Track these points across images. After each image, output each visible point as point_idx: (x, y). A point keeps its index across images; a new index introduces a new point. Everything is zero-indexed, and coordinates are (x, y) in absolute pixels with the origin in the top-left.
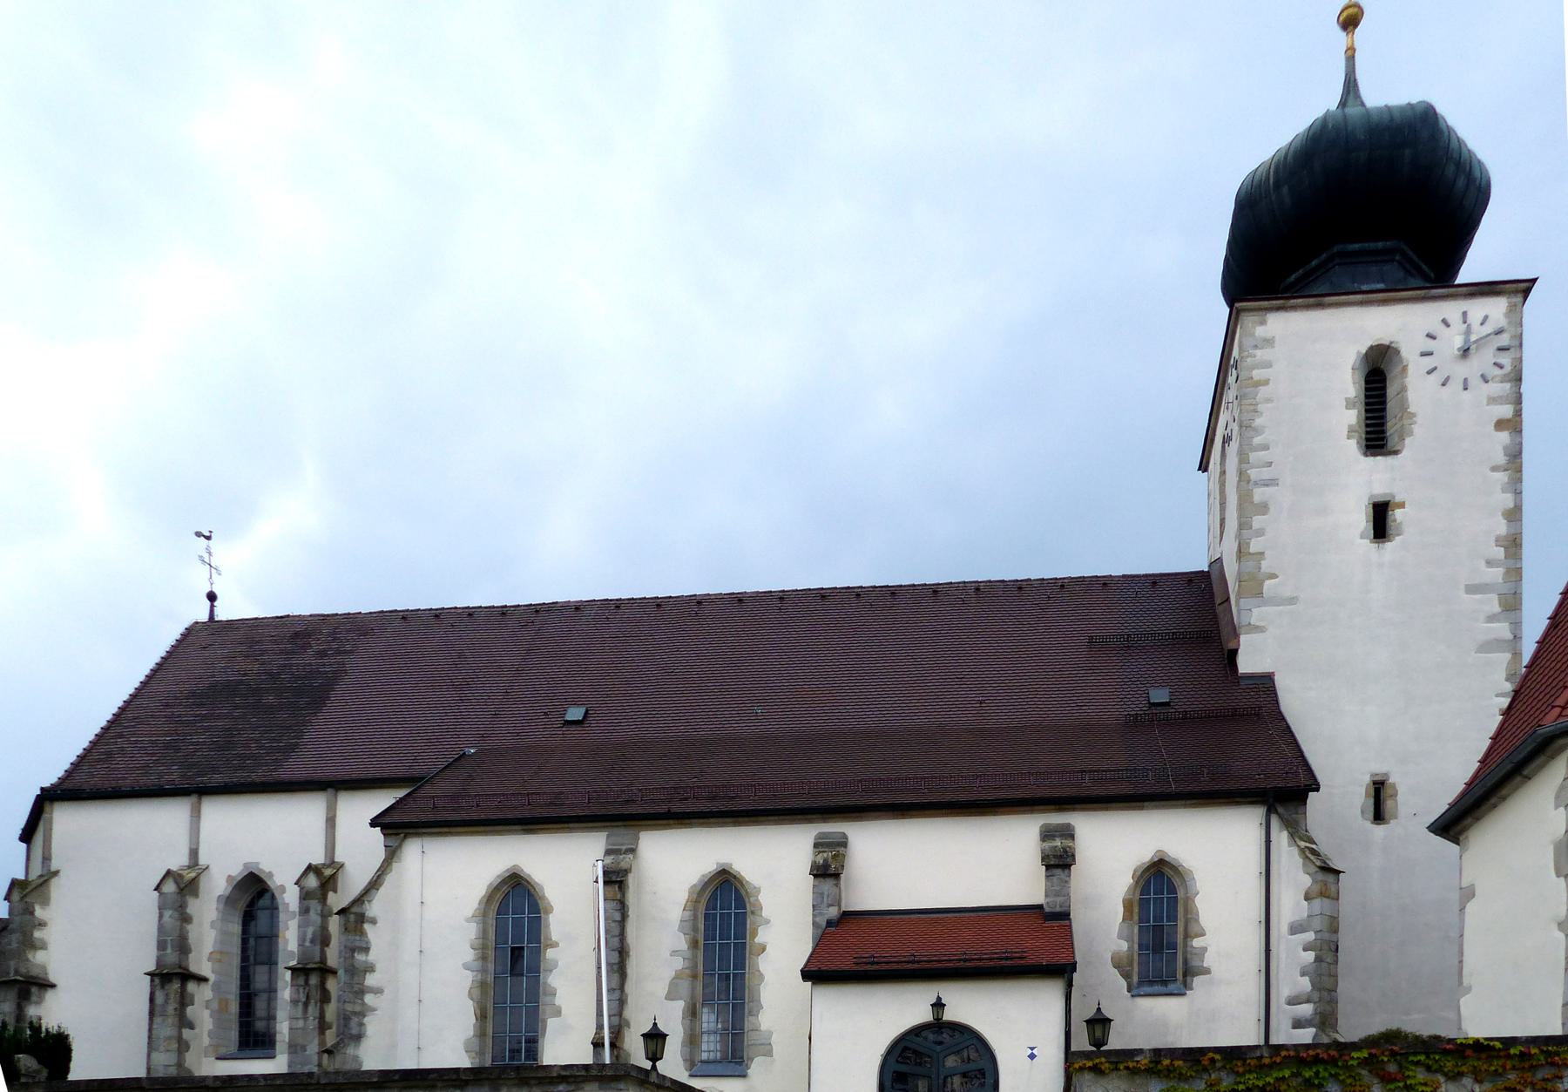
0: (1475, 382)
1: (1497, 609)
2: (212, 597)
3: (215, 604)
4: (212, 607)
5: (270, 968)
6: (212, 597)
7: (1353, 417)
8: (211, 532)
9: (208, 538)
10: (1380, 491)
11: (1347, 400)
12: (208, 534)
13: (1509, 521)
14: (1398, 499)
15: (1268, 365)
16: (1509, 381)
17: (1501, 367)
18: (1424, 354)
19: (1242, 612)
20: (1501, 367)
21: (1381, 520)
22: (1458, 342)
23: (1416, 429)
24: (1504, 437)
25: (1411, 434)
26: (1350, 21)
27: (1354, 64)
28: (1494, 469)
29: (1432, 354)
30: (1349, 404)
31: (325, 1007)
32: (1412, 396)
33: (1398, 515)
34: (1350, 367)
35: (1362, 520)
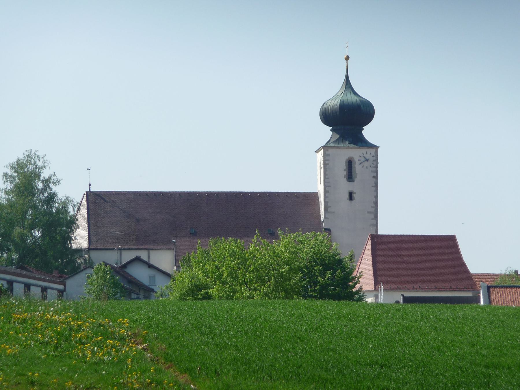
0: (369, 167)
1: (373, 217)
2: (90, 185)
3: (91, 186)
4: (90, 187)
5: (365, 161)
6: (90, 185)
7: (345, 173)
8: (5, 167)
9: (90, 170)
10: (351, 189)
11: (344, 169)
12: (89, 169)
13: (374, 178)
14: (354, 192)
15: (329, 160)
16: (375, 167)
17: (374, 164)
18: (359, 160)
19: (365, 160)
20: (374, 164)
21: (351, 196)
22: (366, 162)
23: (357, 176)
24: (374, 179)
25: (356, 177)
26: (347, 58)
27: (376, 197)
28: (373, 187)
29: (329, 160)
30: (345, 170)
31: (366, 161)
32: (357, 169)
33: (354, 195)
34: (353, 156)
35: (347, 196)
